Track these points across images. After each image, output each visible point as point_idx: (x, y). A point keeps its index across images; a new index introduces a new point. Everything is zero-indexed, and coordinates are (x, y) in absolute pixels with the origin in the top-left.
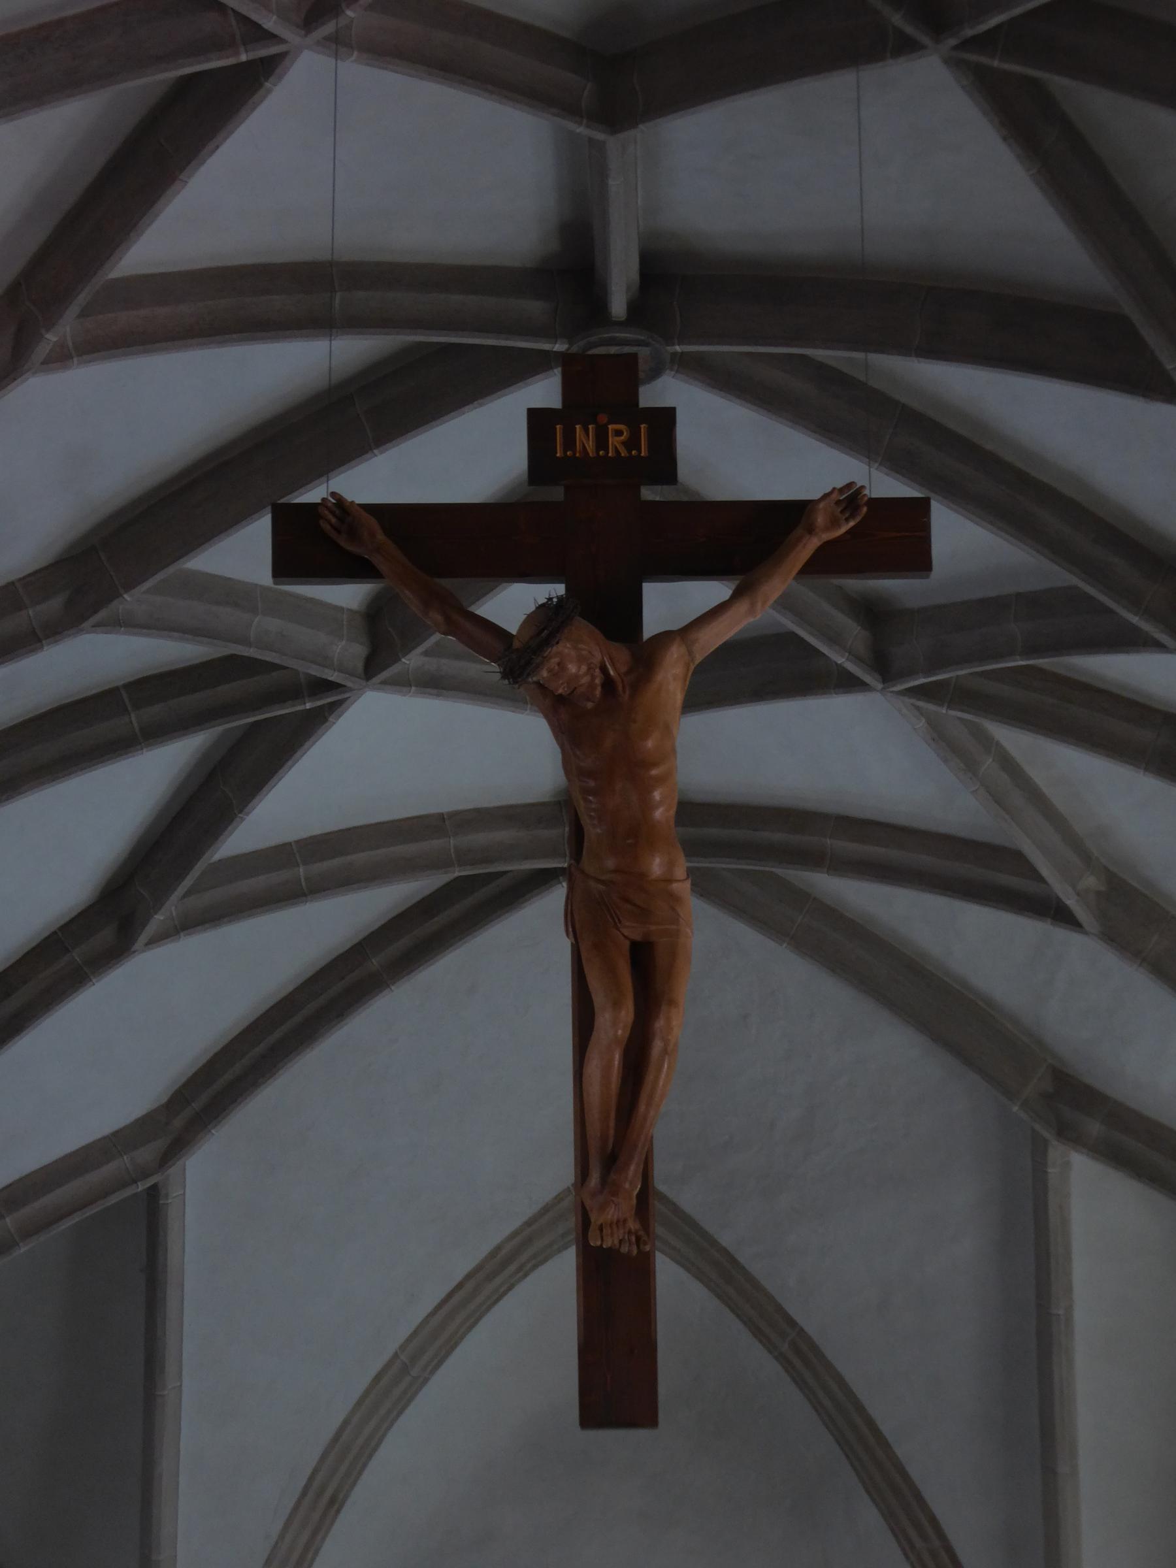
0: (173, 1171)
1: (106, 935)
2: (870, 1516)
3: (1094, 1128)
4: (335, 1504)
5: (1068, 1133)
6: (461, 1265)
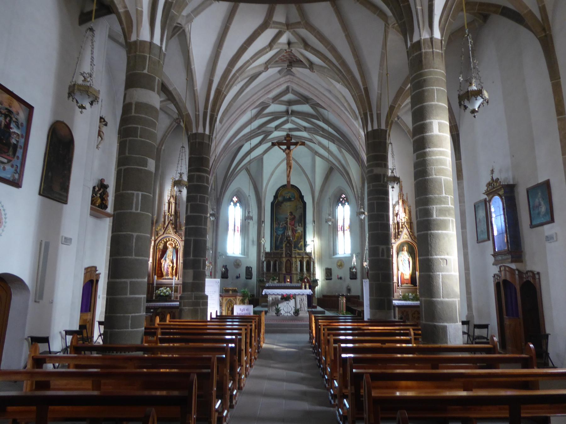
1: (260, 144)
3: (317, 154)
4: (273, 175)
5: (316, 155)
6: (281, 160)
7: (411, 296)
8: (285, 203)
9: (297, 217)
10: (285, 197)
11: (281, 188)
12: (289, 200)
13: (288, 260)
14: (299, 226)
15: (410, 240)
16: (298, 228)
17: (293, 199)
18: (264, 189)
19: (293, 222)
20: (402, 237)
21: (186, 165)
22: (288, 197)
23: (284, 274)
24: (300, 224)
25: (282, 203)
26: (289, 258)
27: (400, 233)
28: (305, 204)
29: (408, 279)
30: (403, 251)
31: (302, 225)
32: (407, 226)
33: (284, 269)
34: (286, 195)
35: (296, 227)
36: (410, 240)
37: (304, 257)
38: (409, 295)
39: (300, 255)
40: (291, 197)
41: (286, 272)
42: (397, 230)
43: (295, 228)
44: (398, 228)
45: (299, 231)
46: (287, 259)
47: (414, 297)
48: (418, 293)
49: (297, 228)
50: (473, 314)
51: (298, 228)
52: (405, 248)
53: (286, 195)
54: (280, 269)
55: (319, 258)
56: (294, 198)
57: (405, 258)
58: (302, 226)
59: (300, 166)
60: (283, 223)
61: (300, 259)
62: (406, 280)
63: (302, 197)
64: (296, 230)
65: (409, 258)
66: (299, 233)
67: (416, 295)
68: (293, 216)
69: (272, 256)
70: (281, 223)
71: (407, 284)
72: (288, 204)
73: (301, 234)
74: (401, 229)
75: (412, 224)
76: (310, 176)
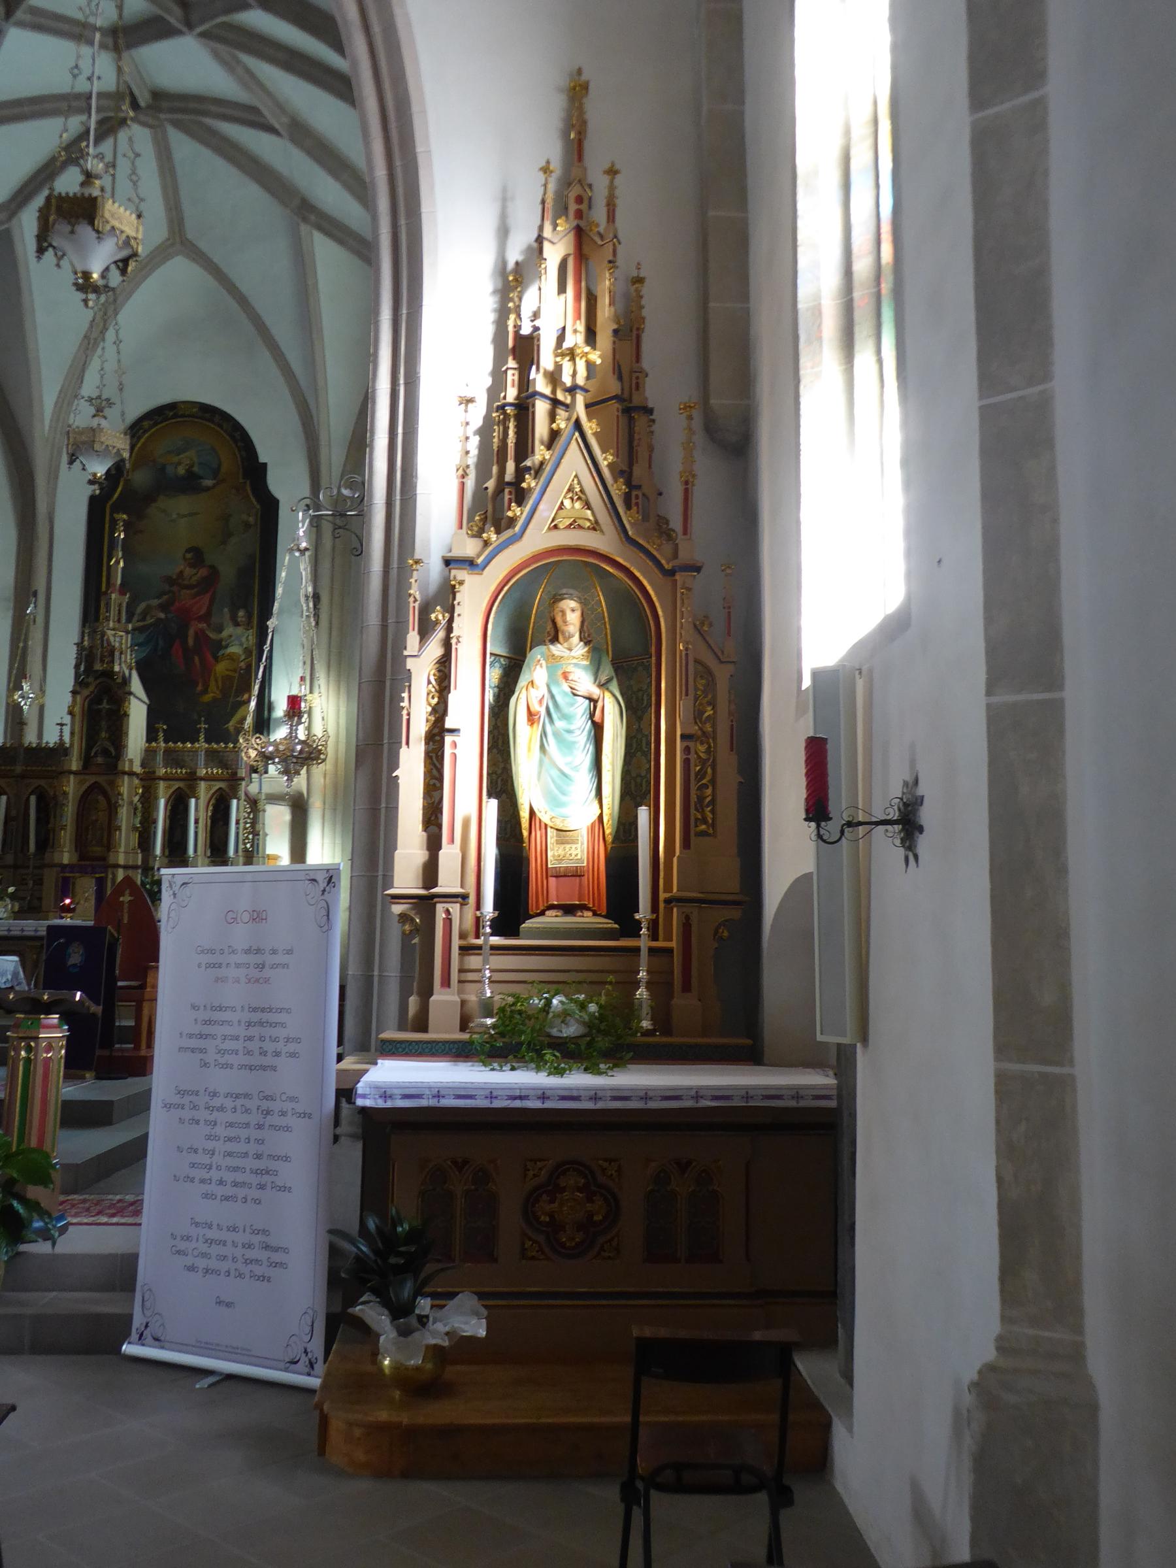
0: (14, 221)
2: (267, 354)
3: (313, 218)
5: (305, 220)
7: (565, 1015)
8: (163, 502)
9: (228, 573)
10: (170, 470)
11: (146, 424)
12: (189, 484)
13: (95, 787)
14: (237, 624)
15: (604, 542)
16: (229, 630)
17: (208, 483)
18: (47, 422)
19: (206, 598)
20: (546, 511)
21: (621, 738)
22: (181, 471)
23: (63, 867)
24: (241, 613)
25: (149, 498)
26: (101, 779)
27: (529, 482)
28: (269, 508)
29: (575, 874)
30: (555, 639)
31: (249, 616)
32: (589, 427)
33: (66, 837)
34: (176, 459)
35: (220, 629)
36: (604, 542)
37: (203, 772)
38: (549, 1002)
39: (178, 764)
40: (196, 469)
41: (82, 857)
42: (510, 466)
43: (212, 635)
44: (524, 448)
45: (234, 649)
46: (91, 779)
47: (594, 1027)
48: (642, 993)
49: (225, 634)
50: (1077, 1354)
51: (229, 630)
52: (571, 614)
53: (176, 459)
54: (46, 842)
55: (335, 794)
56: (215, 473)
57: (561, 690)
58: (248, 625)
59: (243, 301)
60: (149, 608)
61: (177, 785)
62: (560, 875)
63: (255, 472)
64: (219, 645)
65: (596, 692)
66: (232, 658)
67: (626, 1008)
68: (203, 572)
69: (19, 769)
70: (143, 606)
71: (569, 910)
72: (181, 505)
73: (242, 665)
74: (540, 453)
75: (641, 421)
76: (294, 357)
